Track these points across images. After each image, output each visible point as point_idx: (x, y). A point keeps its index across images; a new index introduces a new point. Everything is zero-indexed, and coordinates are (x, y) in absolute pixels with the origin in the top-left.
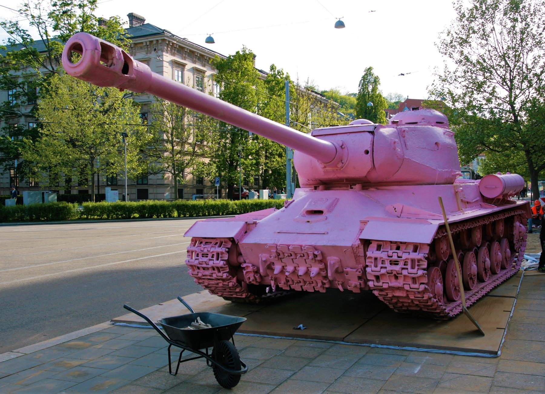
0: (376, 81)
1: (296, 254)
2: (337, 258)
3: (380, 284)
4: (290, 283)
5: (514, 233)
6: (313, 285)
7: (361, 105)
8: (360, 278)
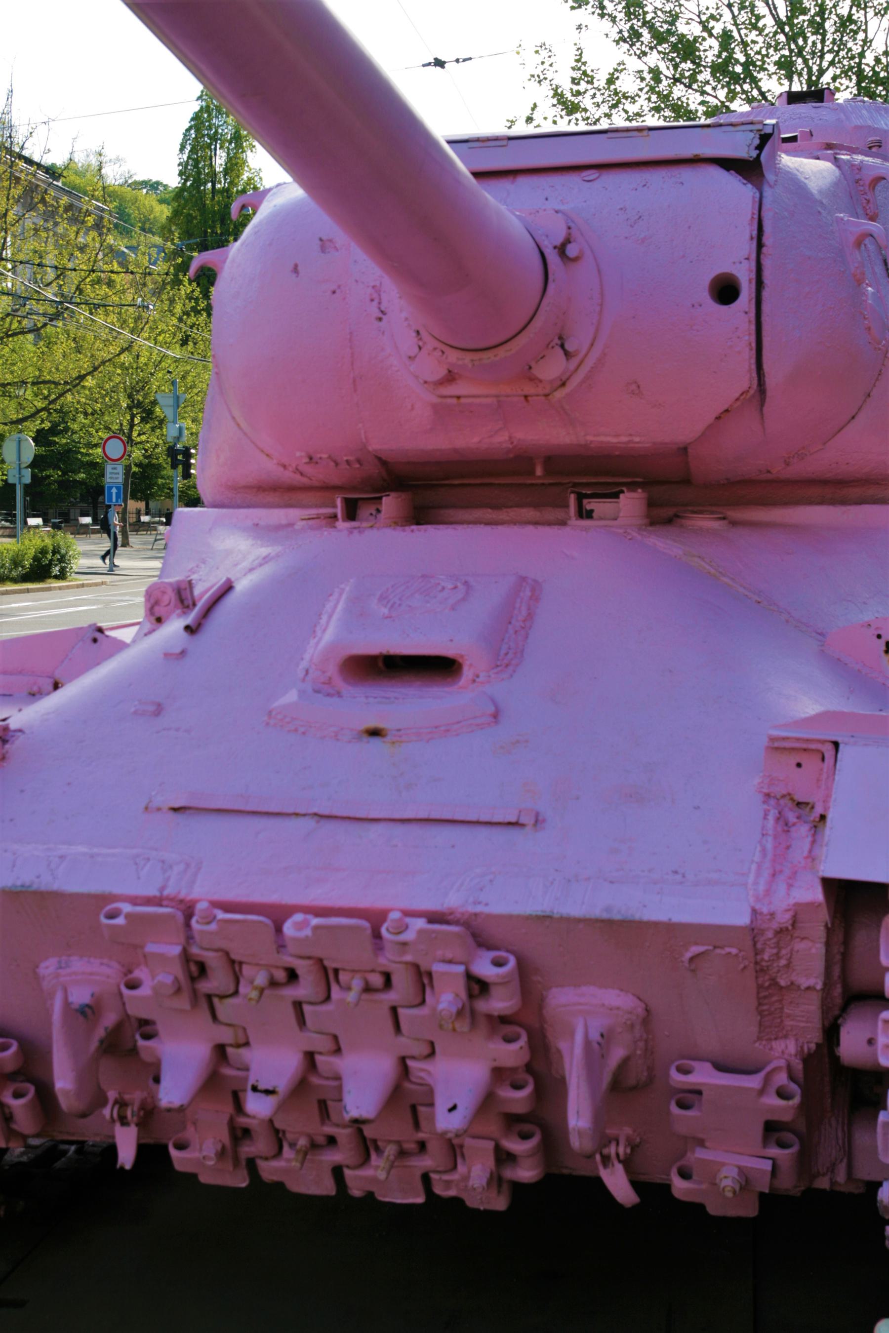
1: (328, 975)
4: (258, 1146)
6: (426, 1162)
7: (190, 218)
8: (772, 1129)
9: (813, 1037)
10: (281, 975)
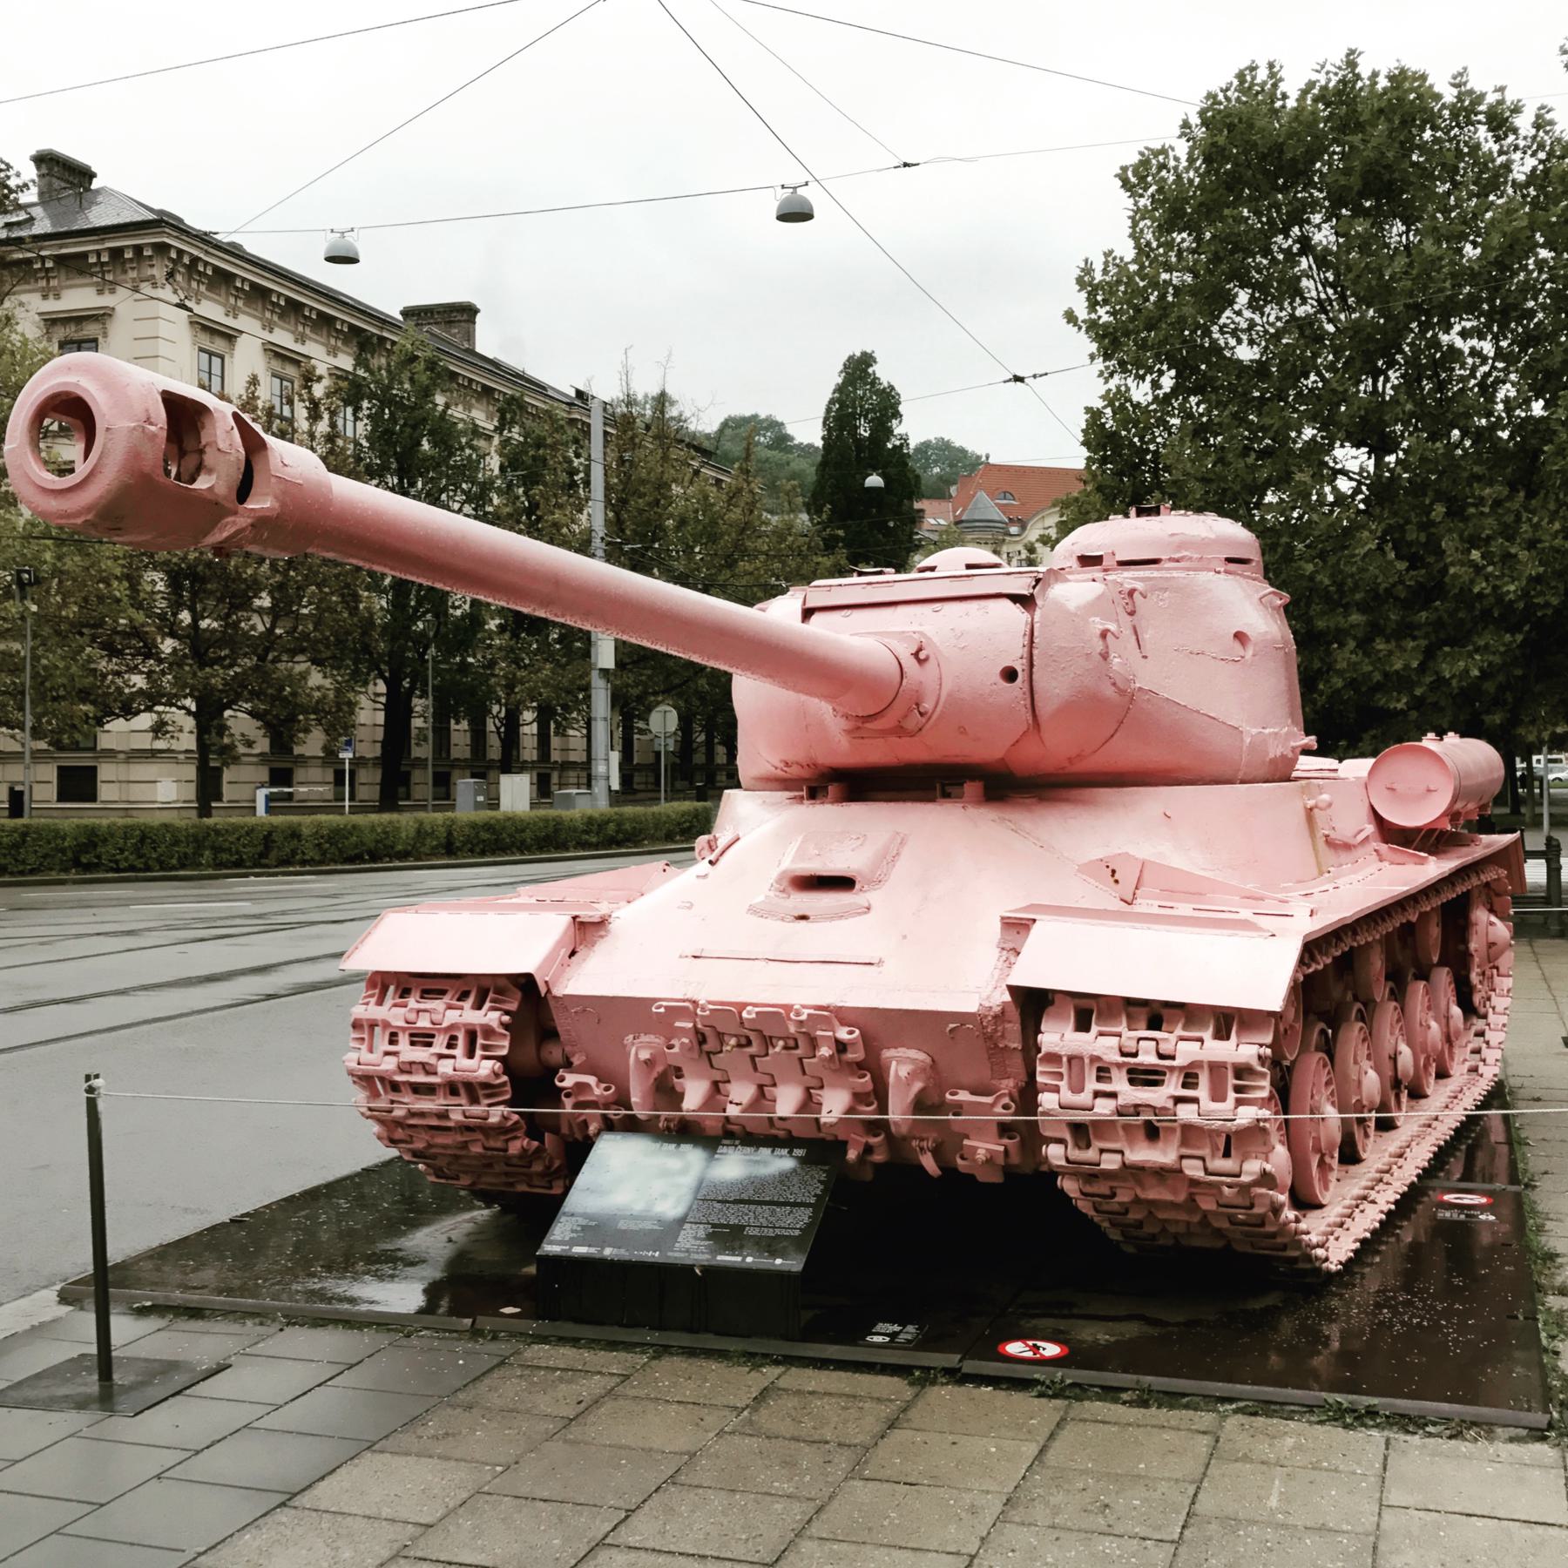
0: (888, 405)
1: (768, 1042)
2: (921, 1056)
3: (1091, 1155)
5: (1473, 946)
9: (1023, 1077)
10: (743, 1041)
